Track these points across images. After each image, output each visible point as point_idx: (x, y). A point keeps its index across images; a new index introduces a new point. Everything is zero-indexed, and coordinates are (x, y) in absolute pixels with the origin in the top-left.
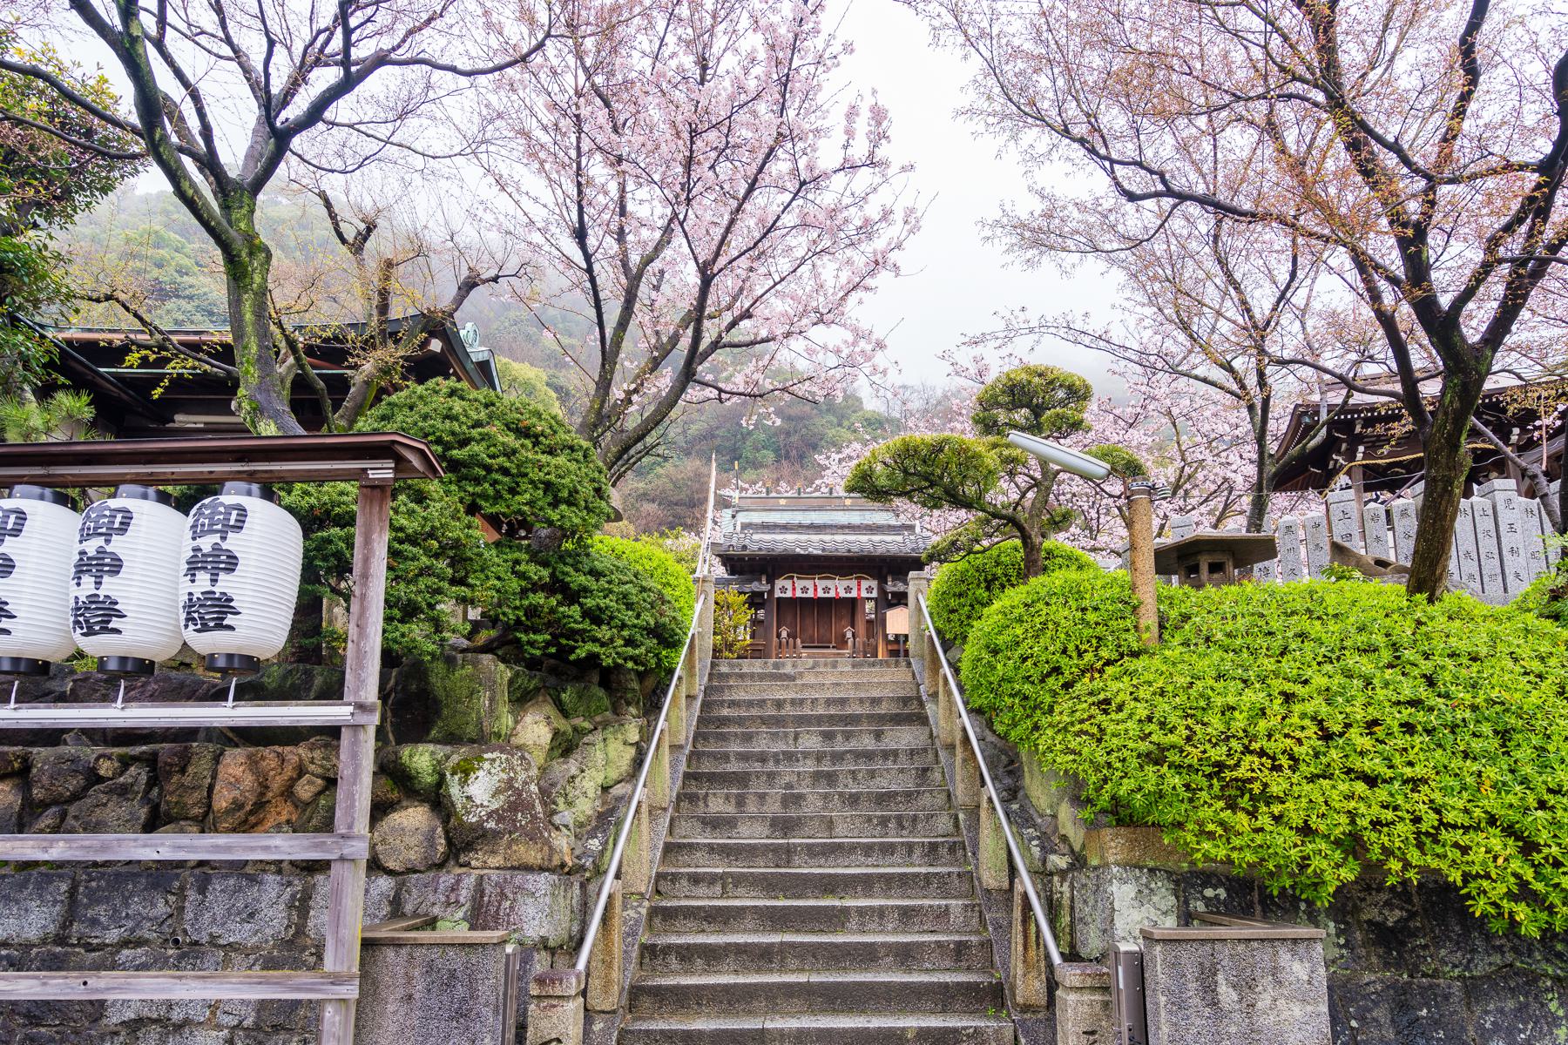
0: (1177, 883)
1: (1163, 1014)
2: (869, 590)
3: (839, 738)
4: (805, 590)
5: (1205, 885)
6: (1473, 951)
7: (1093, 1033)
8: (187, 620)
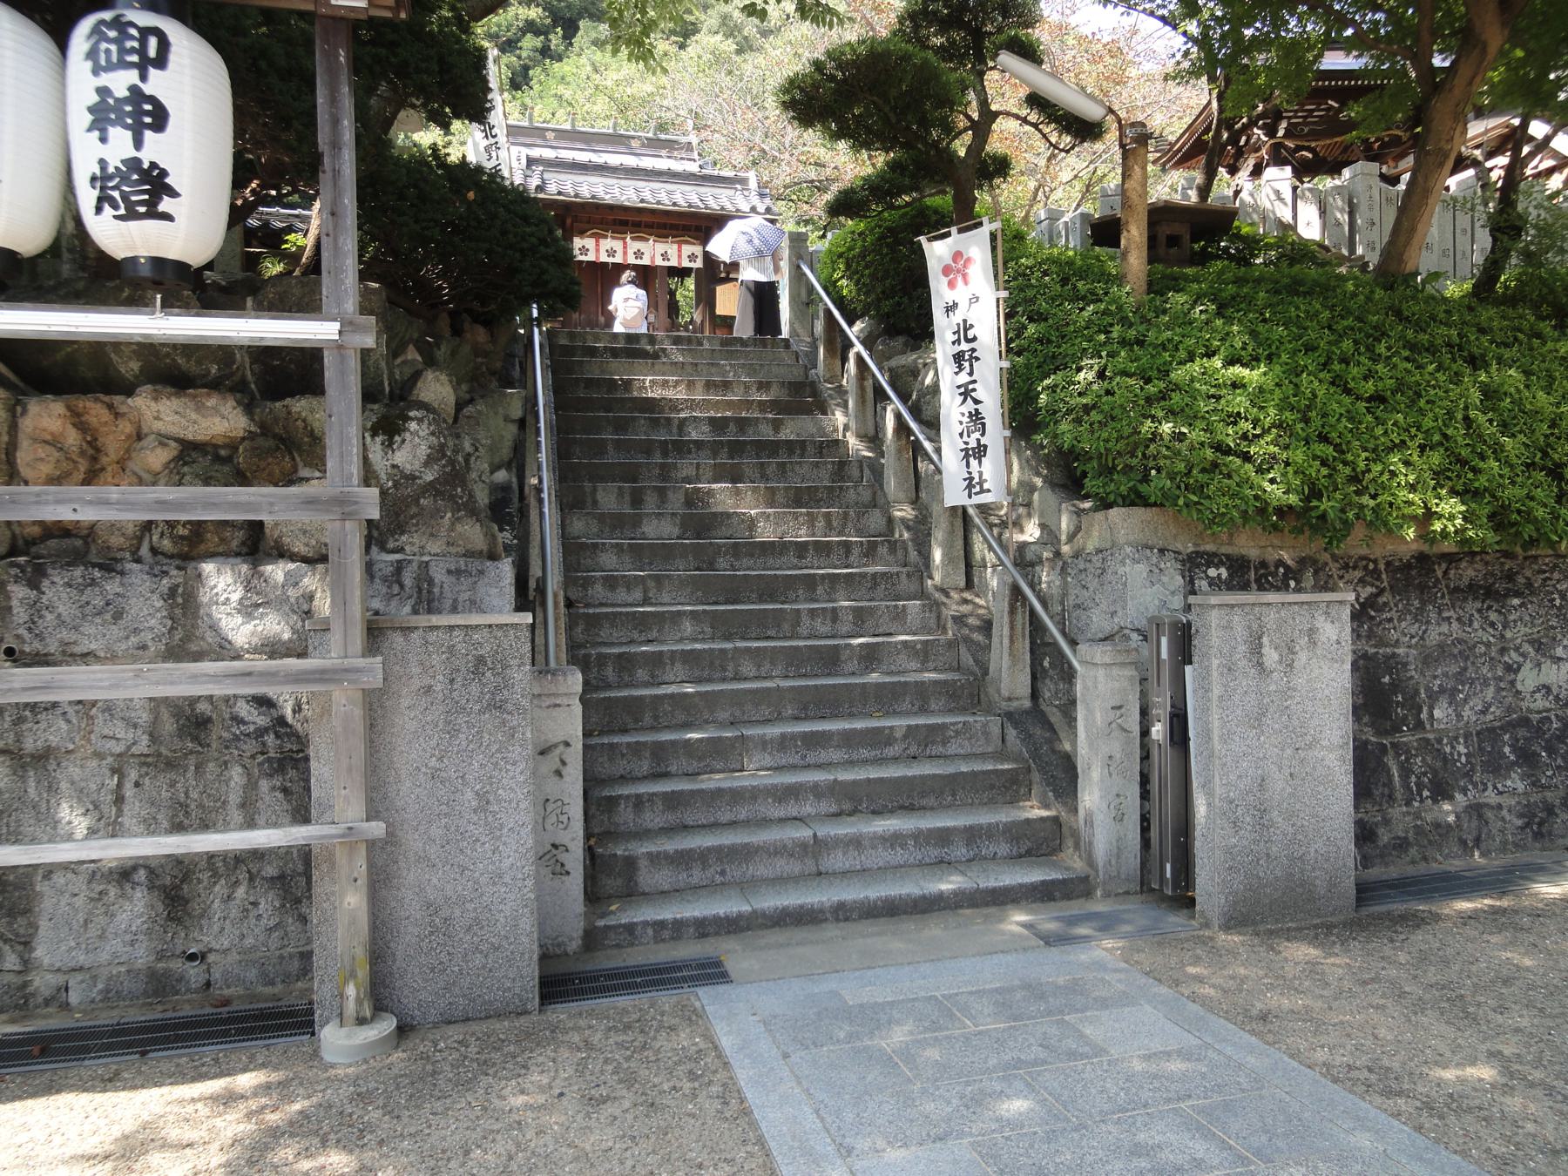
0: (1183, 562)
1: (1215, 674)
2: (692, 257)
3: (732, 427)
4: (611, 253)
5: (1209, 565)
6: (1428, 622)
7: (1120, 707)
8: (100, 200)
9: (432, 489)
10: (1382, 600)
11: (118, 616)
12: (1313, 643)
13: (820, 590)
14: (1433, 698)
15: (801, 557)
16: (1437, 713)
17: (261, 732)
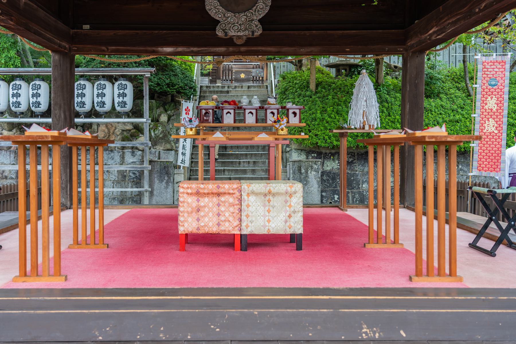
9: (161, 138)
10: (354, 161)
11: (113, 159)
12: (312, 168)
13: (248, 157)
14: (363, 183)
15: (247, 149)
16: (364, 186)
17: (134, 178)
